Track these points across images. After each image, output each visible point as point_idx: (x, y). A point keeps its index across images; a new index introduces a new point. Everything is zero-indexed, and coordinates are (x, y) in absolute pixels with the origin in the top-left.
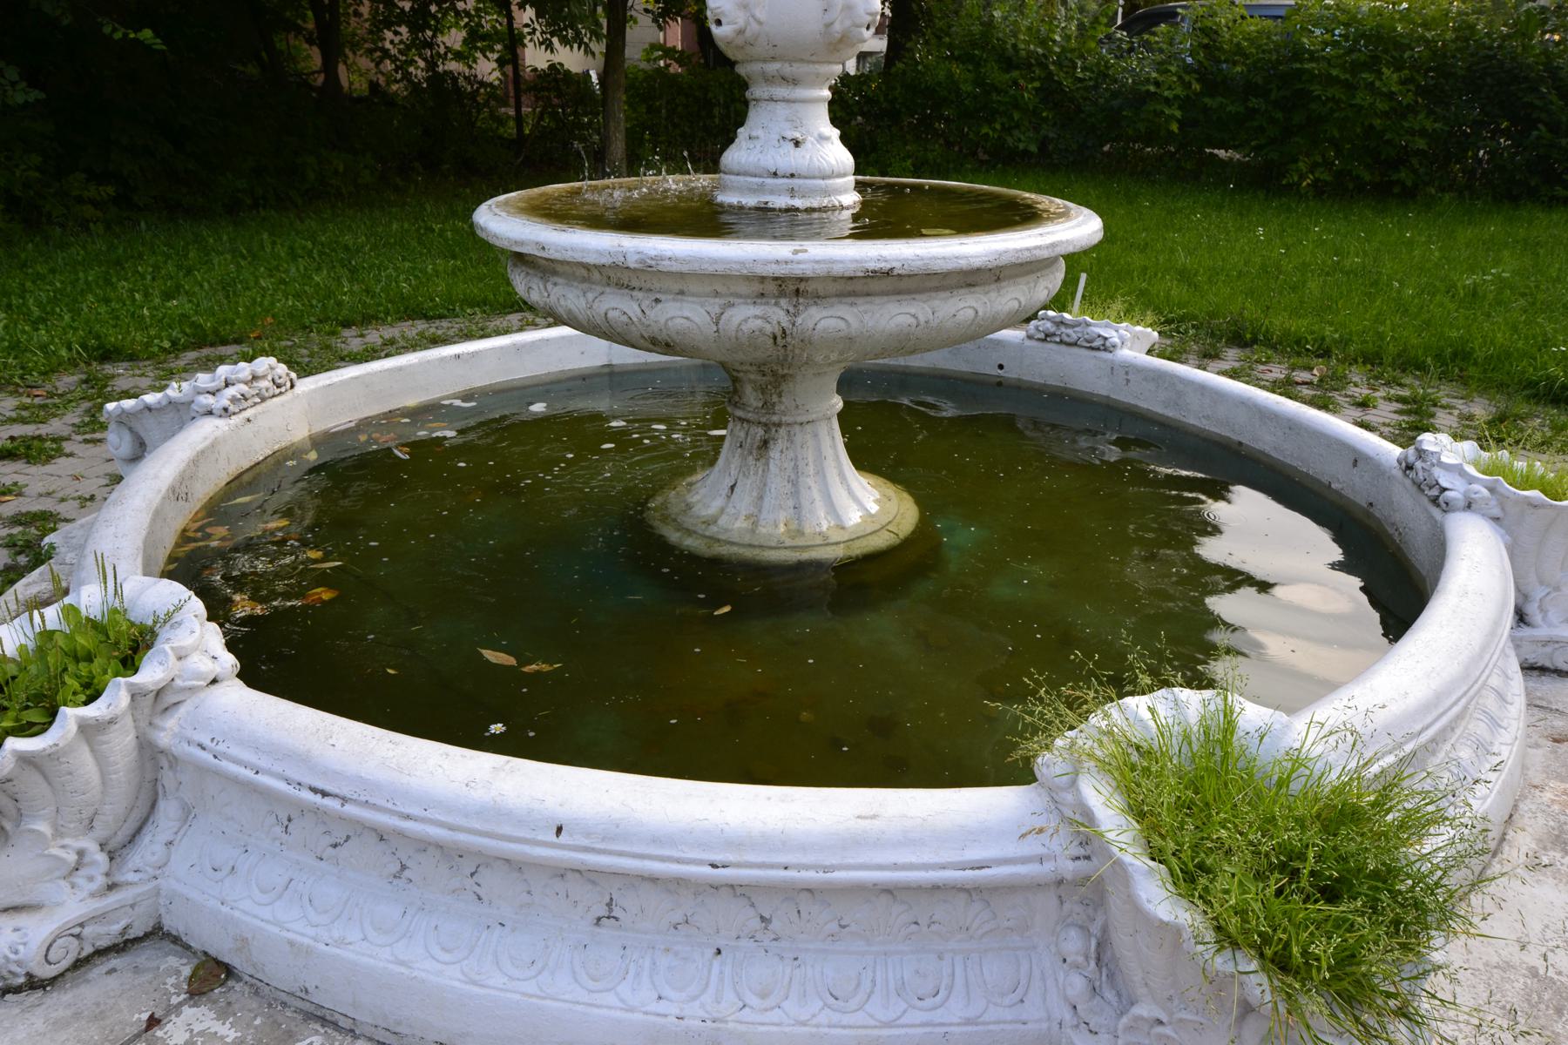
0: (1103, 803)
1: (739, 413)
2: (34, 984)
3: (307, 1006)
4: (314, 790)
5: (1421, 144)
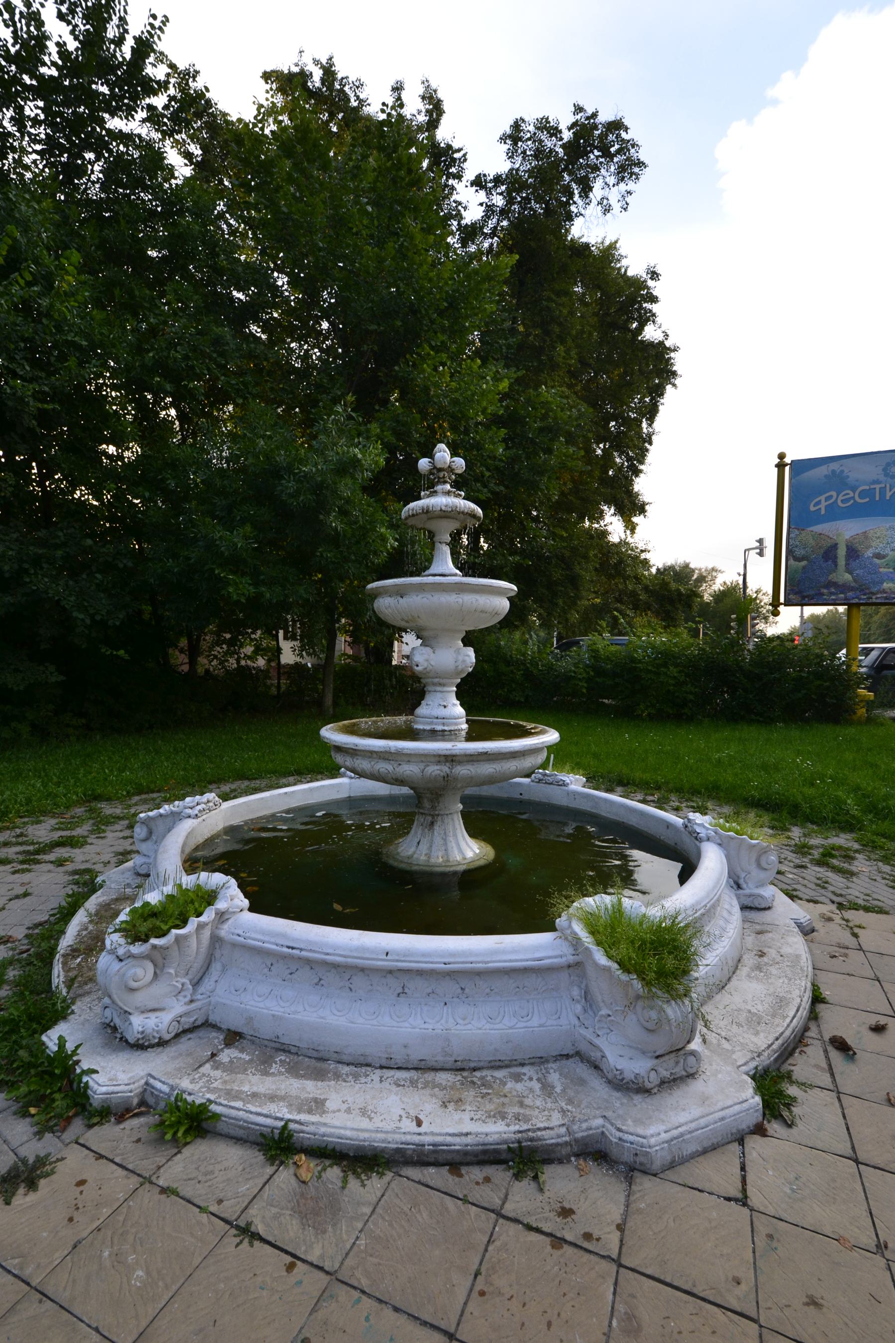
0: (579, 929)
1: (421, 811)
2: (162, 1043)
3: (277, 1045)
4: (288, 947)
5: (691, 697)
